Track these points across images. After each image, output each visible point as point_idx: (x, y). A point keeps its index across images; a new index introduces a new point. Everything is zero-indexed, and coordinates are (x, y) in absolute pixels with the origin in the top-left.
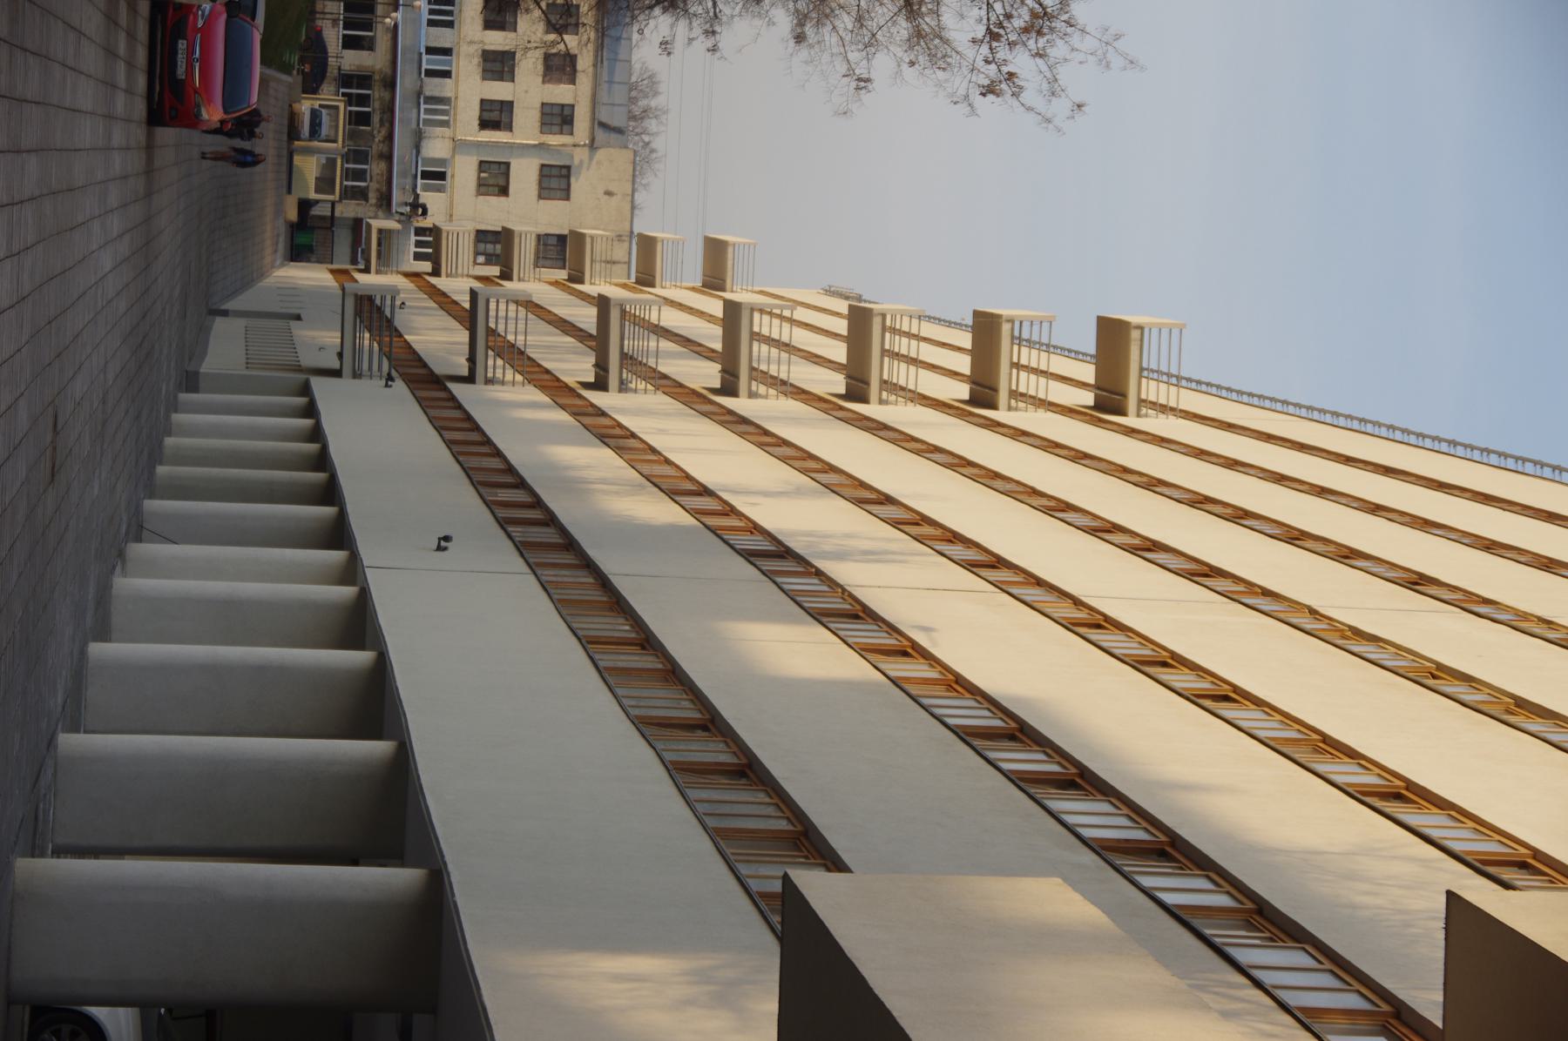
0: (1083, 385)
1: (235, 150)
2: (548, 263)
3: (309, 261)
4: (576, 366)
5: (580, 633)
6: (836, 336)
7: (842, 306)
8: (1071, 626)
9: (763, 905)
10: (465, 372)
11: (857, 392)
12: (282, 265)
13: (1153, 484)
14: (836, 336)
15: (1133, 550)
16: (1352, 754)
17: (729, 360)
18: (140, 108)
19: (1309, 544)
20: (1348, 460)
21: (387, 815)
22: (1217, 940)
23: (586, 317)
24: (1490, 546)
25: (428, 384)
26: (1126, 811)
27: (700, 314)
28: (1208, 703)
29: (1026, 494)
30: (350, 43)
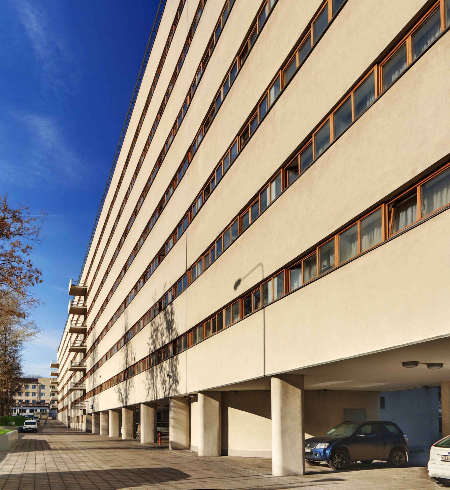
0: (80, 298)
1: (43, 446)
2: (397, 374)
3: (282, 387)
4: (79, 375)
5: (275, 298)
6: (73, 317)
7: (70, 335)
8: (107, 303)
9: (227, 326)
10: (82, 373)
11: (84, 351)
12: (57, 419)
13: (119, 247)
14: (73, 317)
15: (126, 271)
16: (120, 307)
17: (77, 351)
18: (46, 452)
19: (96, 321)
20: (99, 243)
21: (118, 411)
22: (269, 107)
23: (70, 373)
24: (243, 53)
25: (179, 344)
26: (269, 183)
27: (71, 338)
28: (126, 306)
29: (190, 95)
30: (25, 412)
